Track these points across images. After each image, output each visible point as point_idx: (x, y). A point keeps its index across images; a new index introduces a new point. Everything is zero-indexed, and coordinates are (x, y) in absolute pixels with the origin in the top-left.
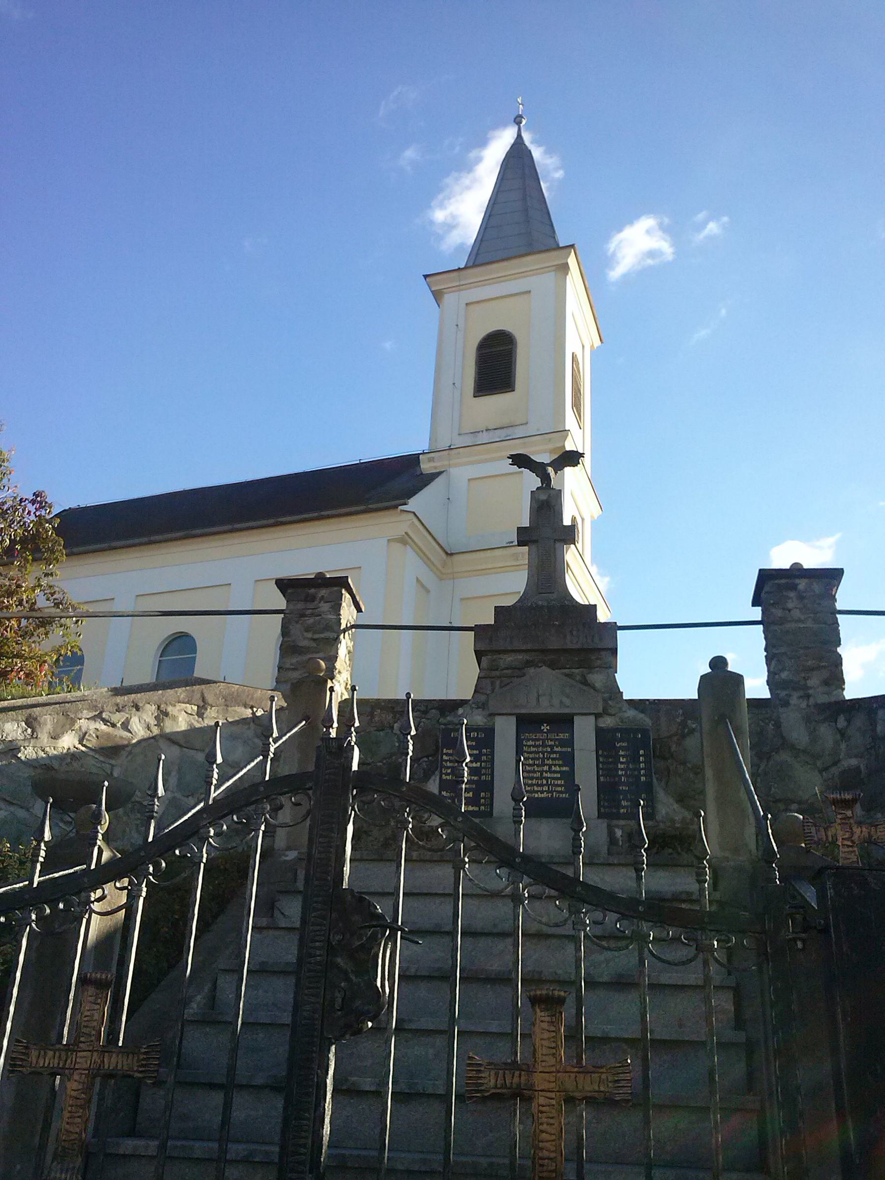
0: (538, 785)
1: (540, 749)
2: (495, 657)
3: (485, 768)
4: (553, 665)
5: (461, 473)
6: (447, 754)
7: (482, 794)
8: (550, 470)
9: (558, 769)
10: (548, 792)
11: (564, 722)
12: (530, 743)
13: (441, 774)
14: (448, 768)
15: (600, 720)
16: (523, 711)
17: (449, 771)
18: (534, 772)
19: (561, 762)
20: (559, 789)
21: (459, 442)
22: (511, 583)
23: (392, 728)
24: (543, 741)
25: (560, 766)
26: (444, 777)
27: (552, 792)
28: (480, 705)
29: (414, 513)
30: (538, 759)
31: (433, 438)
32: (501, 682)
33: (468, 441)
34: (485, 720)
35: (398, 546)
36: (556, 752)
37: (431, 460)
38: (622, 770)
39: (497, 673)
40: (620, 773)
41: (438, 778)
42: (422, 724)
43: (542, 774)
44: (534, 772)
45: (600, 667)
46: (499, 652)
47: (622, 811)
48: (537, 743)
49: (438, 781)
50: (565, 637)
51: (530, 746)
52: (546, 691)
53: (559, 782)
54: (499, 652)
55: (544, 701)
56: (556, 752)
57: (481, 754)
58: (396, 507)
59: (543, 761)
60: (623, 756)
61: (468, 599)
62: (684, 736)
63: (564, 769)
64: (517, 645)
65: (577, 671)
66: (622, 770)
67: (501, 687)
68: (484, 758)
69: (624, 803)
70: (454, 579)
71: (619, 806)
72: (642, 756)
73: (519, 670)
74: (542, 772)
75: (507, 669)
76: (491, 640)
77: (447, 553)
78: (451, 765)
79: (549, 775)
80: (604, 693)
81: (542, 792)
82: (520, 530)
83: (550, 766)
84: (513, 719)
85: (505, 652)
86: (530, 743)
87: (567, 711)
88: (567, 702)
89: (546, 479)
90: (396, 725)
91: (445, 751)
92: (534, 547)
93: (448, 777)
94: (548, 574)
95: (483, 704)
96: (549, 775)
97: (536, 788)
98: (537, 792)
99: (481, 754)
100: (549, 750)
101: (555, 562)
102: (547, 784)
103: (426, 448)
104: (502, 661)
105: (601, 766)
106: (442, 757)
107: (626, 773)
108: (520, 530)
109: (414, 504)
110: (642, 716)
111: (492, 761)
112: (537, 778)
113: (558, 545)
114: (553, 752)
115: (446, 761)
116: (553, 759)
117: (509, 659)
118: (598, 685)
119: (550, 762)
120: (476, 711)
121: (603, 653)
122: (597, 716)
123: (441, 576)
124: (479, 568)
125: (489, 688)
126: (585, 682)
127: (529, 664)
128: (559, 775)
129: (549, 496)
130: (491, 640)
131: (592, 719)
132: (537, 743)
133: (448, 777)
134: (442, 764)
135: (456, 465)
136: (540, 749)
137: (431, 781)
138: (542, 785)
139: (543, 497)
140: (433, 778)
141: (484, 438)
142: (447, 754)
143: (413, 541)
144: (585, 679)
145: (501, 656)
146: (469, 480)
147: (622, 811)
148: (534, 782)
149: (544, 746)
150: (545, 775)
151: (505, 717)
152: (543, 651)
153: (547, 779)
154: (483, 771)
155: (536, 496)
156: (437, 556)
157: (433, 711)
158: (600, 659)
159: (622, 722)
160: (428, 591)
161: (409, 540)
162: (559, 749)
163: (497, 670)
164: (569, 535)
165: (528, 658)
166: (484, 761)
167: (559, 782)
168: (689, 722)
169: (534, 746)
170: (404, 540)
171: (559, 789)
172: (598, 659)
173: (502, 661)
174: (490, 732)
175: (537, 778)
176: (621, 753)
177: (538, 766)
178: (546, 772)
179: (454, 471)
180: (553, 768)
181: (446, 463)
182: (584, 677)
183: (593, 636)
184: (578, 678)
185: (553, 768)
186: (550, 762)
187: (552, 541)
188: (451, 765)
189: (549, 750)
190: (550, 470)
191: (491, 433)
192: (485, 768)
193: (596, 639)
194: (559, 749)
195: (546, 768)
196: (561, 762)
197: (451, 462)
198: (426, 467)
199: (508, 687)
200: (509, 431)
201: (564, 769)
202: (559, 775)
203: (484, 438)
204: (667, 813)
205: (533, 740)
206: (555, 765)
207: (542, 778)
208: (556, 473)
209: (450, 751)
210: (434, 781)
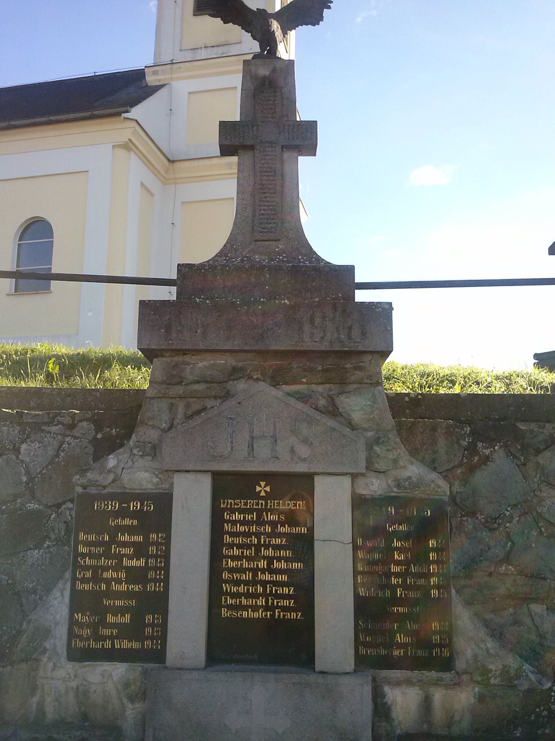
0: (248, 595)
1: (254, 529)
2: (176, 359)
3: (156, 568)
4: (276, 379)
5: (182, 86)
6: (87, 544)
7: (149, 618)
8: (275, 26)
9: (283, 565)
10: (266, 608)
11: (300, 485)
12: (237, 516)
13: (74, 579)
14: (86, 568)
15: (361, 481)
16: (225, 467)
17: (89, 574)
18: (242, 570)
19: (288, 553)
20: (286, 603)
21: (180, 57)
22: (206, 219)
23: (17, 451)
24: (260, 513)
25: (287, 560)
26: (79, 586)
27: (272, 608)
28: (148, 450)
29: (136, 121)
30: (249, 547)
31: (157, 53)
32: (188, 406)
33: (188, 56)
34: (155, 480)
35: (122, 152)
36: (280, 535)
37: (155, 73)
38: (397, 575)
39: (180, 390)
40: (394, 581)
41: (68, 586)
42: (65, 446)
43: (255, 575)
44: (242, 570)
45: (360, 382)
46: (185, 352)
47: (396, 653)
48: (249, 517)
49: (67, 594)
50: (301, 328)
51: (234, 523)
52: (268, 428)
53: (286, 590)
54: (185, 352)
55: (263, 449)
56: (280, 535)
57: (147, 543)
58: (119, 114)
59: (258, 550)
60: (400, 550)
61: (189, 202)
62: (472, 469)
63: (296, 566)
64: (215, 341)
65: (320, 388)
66: (397, 575)
67: (188, 417)
68: (152, 550)
69: (400, 638)
70: (175, 184)
71: (391, 644)
72: (433, 550)
73: (220, 387)
74: (254, 571)
75: (198, 382)
76: (168, 328)
77: (169, 160)
78: (94, 562)
79: (267, 577)
80: (365, 430)
81: (255, 608)
82: (224, 125)
83: (270, 560)
84: (206, 482)
85: (196, 352)
86: (237, 516)
87: (301, 468)
88: (303, 451)
89: (268, 43)
90: (24, 446)
91: (82, 536)
92: (247, 156)
93: (86, 587)
94: (269, 208)
95: (154, 447)
96: (267, 577)
97: (244, 601)
98: (245, 608)
99: (147, 543)
100: (268, 529)
101: (282, 186)
102: (265, 595)
103: (151, 62)
104: (188, 369)
105: (360, 555)
106: (76, 549)
107: (404, 581)
108: (224, 125)
109: (136, 112)
110: (433, 476)
111: (167, 557)
112: (246, 583)
113: (287, 155)
114: (274, 534)
115: (83, 556)
116: (277, 547)
117: (202, 364)
118: (357, 416)
119: (270, 552)
120: (140, 462)
121: (367, 358)
122: (354, 476)
123: (165, 181)
124: (198, 174)
125: (165, 417)
126: (333, 411)
127: (235, 373)
128: (285, 578)
129: (274, 70)
130: (168, 328)
131: (347, 481)
132: (249, 517)
133: (86, 587)
134: (75, 561)
135: (178, 79)
136: (254, 529)
137: (56, 593)
138: (256, 596)
139: (263, 71)
140: (60, 585)
141: (203, 54)
142: (87, 544)
143: (137, 148)
144: (334, 405)
145: (187, 358)
146: (190, 93)
147: (396, 653)
148: (241, 589)
149: (260, 522)
150: (260, 576)
151: (191, 477)
152: (262, 354)
153: (264, 584)
154: (151, 574)
155: (253, 69)
156: (160, 162)
157: (85, 424)
158: (360, 368)
159: (399, 486)
160: (152, 195)
161: (134, 148)
162: (286, 529)
163: (180, 383)
164: (305, 138)
165: (234, 363)
166: (152, 556)
167: (286, 590)
168: (480, 445)
169: (243, 523)
170: (128, 146)
171: (286, 603)
172: (355, 368)
173: (188, 369)
174: (164, 502)
175: (246, 583)
176: (396, 544)
177: (249, 559)
178: (263, 571)
179: (175, 84)
180: (276, 565)
181: (168, 76)
182: (332, 400)
183: (350, 328)
184: (322, 402)
185: (276, 565)
186: (270, 552)
187: (278, 149)
188: (94, 562)
189: (268, 529)
190: (275, 26)
191: (209, 50)
192: (156, 568)
193: (356, 333)
194: (286, 529)
195: (262, 564)
196: (288, 553)
197: (173, 76)
198: (151, 79)
199: (198, 420)
200: (225, 49)
201: (296, 566)
202: (285, 578)
203: (203, 54)
204: (475, 656)
205: (241, 511)
206: (279, 559)
207: (254, 582)
208: (285, 33)
209: (92, 538)
210: (62, 591)
